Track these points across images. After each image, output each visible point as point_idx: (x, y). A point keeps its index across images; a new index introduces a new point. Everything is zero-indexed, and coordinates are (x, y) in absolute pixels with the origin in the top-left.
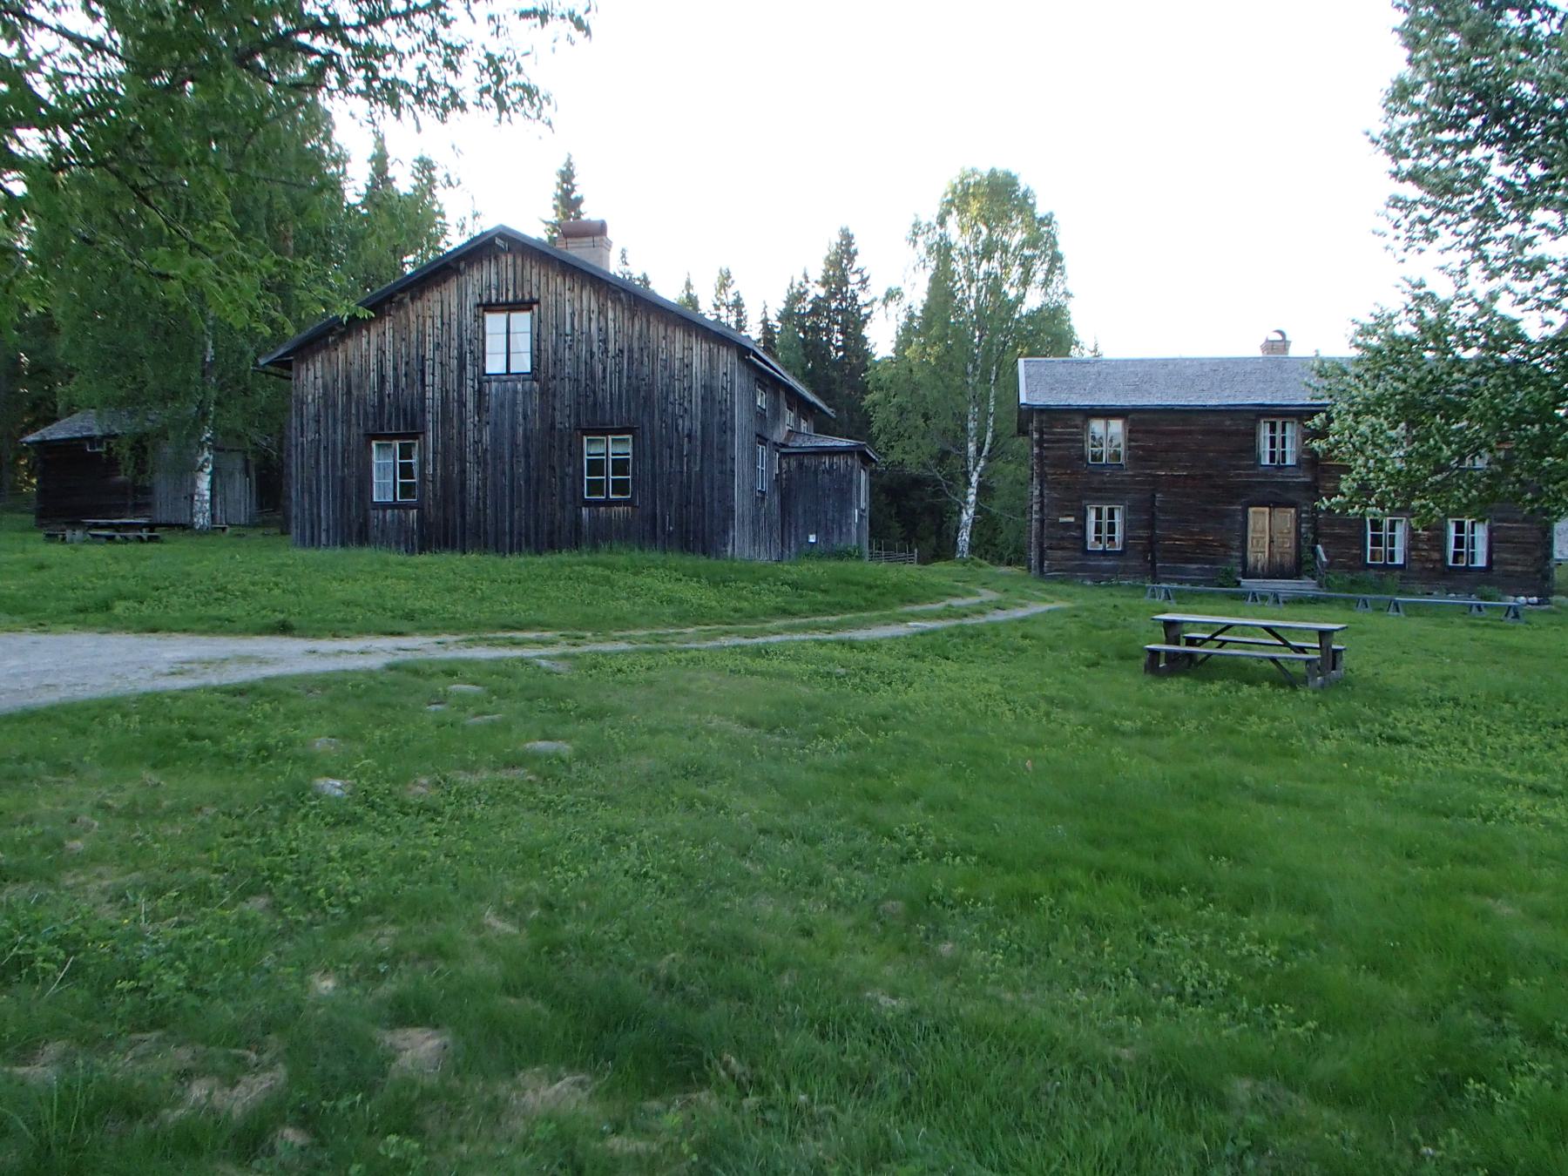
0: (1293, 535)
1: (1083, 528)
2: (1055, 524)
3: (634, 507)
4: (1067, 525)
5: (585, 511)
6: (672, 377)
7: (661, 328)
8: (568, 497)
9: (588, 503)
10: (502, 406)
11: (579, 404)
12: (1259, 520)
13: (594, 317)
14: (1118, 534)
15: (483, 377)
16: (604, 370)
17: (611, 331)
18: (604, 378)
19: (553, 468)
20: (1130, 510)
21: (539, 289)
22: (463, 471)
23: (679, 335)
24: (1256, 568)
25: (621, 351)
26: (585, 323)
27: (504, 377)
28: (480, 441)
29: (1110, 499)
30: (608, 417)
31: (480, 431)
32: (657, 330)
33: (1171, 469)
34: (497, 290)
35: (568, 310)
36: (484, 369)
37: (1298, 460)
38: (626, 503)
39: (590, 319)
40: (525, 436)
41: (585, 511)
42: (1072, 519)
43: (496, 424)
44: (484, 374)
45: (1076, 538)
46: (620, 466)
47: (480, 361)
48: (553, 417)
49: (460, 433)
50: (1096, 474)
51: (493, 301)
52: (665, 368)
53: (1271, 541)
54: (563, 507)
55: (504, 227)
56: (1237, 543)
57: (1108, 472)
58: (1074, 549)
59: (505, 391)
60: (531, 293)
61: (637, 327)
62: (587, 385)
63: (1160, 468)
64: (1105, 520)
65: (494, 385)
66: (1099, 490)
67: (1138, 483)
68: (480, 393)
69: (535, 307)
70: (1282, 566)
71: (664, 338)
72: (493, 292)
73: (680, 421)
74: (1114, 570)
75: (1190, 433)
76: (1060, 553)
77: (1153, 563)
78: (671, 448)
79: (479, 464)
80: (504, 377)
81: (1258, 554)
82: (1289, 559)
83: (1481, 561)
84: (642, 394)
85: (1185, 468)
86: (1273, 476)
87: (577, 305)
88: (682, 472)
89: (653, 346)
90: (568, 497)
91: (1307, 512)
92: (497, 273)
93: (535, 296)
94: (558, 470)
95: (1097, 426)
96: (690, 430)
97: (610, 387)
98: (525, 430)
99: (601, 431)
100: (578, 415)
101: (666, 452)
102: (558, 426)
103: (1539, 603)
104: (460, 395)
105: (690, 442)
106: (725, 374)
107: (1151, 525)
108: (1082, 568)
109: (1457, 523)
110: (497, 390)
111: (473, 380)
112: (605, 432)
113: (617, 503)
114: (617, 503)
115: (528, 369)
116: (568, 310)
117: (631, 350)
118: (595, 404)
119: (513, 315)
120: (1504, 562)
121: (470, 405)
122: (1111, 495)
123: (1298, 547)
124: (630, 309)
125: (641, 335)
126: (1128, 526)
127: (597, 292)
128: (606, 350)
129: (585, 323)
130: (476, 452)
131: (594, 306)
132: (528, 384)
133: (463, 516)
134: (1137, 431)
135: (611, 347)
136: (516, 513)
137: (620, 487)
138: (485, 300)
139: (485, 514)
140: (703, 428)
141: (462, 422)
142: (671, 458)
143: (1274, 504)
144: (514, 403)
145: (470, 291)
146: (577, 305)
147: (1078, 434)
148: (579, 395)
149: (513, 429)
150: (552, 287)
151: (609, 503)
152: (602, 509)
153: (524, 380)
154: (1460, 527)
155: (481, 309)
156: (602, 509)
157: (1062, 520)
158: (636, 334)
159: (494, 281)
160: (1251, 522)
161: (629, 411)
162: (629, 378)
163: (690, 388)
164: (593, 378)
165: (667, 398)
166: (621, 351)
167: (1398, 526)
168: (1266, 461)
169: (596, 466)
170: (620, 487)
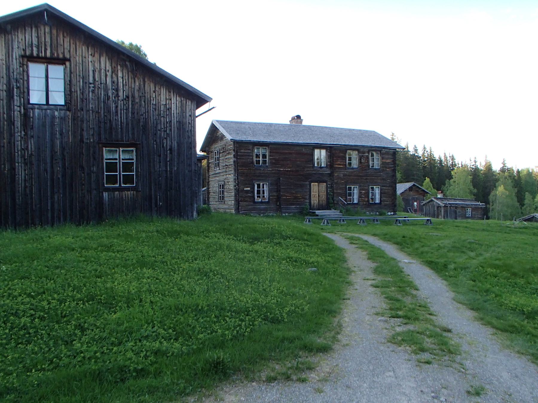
0: (325, 193)
1: (253, 192)
2: (243, 190)
3: (137, 191)
4: (247, 192)
5: (105, 195)
6: (159, 115)
7: (152, 86)
8: (93, 186)
9: (107, 190)
10: (44, 125)
11: (100, 127)
12: (315, 187)
13: (109, 74)
14: (266, 195)
15: (27, 105)
16: (117, 107)
17: (121, 85)
18: (117, 112)
19: (83, 168)
20: (271, 184)
21: (69, 51)
22: (13, 169)
23: (163, 91)
24: (314, 206)
25: (128, 97)
26: (103, 77)
27: (46, 107)
28: (27, 149)
29: (263, 180)
30: (120, 137)
31: (26, 142)
32: (150, 87)
33: (285, 168)
34: (38, 48)
35: (91, 68)
36: (29, 100)
37: (326, 165)
38: (133, 189)
39: (106, 76)
40: (63, 148)
41: (105, 195)
42: (249, 189)
43: (39, 137)
44: (29, 103)
45: (251, 197)
46: (127, 166)
47: (26, 94)
48: (82, 135)
49: (9, 143)
50: (258, 170)
51: (35, 54)
52: (155, 110)
53: (319, 196)
54: (90, 192)
55: (48, 5)
56: (308, 197)
57: (262, 169)
58: (250, 201)
59: (46, 116)
60: (63, 53)
61: (137, 84)
62: (105, 116)
63: (281, 168)
64: (261, 189)
65: (37, 111)
66: (259, 176)
67: (274, 173)
68: (26, 116)
69: (68, 64)
70: (322, 205)
71: (154, 92)
72: (35, 49)
73: (165, 141)
74: (266, 210)
75: (291, 154)
76: (245, 203)
77: (280, 205)
78: (160, 156)
79: (26, 164)
80: (46, 107)
81: (315, 201)
82: (324, 203)
83: (377, 201)
84: (141, 124)
85: (290, 167)
86: (318, 171)
87: (97, 65)
88: (166, 171)
89: (147, 96)
90: (93, 186)
91: (330, 185)
92: (38, 37)
93: (67, 56)
94: (86, 168)
95: (317, 152)
96: (171, 146)
97: (122, 117)
98: (61, 143)
99: (115, 144)
100: (99, 134)
101: (157, 158)
102: (85, 141)
103: (394, 215)
104: (9, 116)
105: (171, 153)
106: (190, 116)
107: (278, 191)
108: (254, 209)
109: (257, 184)
110: (39, 115)
111: (20, 107)
112: (118, 146)
113: (128, 189)
114: (128, 189)
115: (63, 103)
116: (91, 68)
117: (133, 97)
118: (111, 128)
119: (51, 67)
120: (384, 201)
121: (18, 124)
122: (264, 178)
123: (328, 199)
124: (132, 72)
125: (140, 88)
126: (270, 191)
127: (111, 59)
128: (117, 96)
129: (103, 77)
130: (23, 156)
131: (109, 67)
132: (63, 112)
133: (14, 199)
134: (273, 152)
135: (121, 94)
136: (56, 197)
137: (128, 179)
138: (28, 53)
139: (32, 198)
140: (178, 145)
141: (12, 135)
142: (160, 162)
143: (319, 182)
144: (52, 125)
145: (15, 46)
146: (97, 65)
147: (250, 153)
148: (100, 122)
149: (52, 141)
150: (79, 52)
151: (121, 189)
152: (117, 193)
153: (61, 110)
154: (259, 186)
155: (26, 60)
156: (117, 193)
157: (245, 189)
158: (137, 88)
159: (35, 42)
160: (312, 189)
161: (133, 134)
162: (133, 113)
163: (171, 121)
164: (109, 111)
165: (156, 127)
166: (128, 97)
167: (265, 186)
168: (316, 165)
169: (112, 167)
170: (128, 179)
